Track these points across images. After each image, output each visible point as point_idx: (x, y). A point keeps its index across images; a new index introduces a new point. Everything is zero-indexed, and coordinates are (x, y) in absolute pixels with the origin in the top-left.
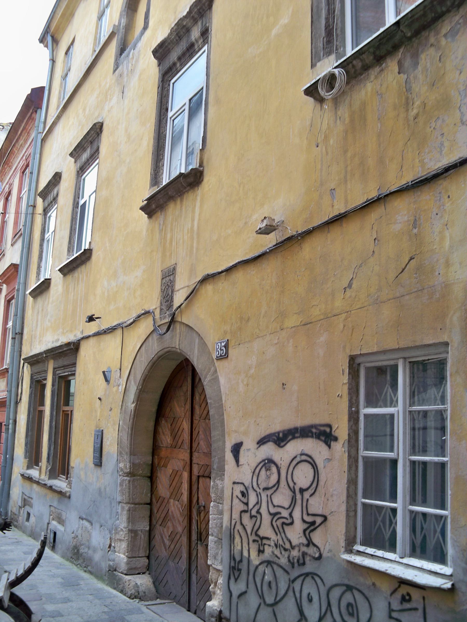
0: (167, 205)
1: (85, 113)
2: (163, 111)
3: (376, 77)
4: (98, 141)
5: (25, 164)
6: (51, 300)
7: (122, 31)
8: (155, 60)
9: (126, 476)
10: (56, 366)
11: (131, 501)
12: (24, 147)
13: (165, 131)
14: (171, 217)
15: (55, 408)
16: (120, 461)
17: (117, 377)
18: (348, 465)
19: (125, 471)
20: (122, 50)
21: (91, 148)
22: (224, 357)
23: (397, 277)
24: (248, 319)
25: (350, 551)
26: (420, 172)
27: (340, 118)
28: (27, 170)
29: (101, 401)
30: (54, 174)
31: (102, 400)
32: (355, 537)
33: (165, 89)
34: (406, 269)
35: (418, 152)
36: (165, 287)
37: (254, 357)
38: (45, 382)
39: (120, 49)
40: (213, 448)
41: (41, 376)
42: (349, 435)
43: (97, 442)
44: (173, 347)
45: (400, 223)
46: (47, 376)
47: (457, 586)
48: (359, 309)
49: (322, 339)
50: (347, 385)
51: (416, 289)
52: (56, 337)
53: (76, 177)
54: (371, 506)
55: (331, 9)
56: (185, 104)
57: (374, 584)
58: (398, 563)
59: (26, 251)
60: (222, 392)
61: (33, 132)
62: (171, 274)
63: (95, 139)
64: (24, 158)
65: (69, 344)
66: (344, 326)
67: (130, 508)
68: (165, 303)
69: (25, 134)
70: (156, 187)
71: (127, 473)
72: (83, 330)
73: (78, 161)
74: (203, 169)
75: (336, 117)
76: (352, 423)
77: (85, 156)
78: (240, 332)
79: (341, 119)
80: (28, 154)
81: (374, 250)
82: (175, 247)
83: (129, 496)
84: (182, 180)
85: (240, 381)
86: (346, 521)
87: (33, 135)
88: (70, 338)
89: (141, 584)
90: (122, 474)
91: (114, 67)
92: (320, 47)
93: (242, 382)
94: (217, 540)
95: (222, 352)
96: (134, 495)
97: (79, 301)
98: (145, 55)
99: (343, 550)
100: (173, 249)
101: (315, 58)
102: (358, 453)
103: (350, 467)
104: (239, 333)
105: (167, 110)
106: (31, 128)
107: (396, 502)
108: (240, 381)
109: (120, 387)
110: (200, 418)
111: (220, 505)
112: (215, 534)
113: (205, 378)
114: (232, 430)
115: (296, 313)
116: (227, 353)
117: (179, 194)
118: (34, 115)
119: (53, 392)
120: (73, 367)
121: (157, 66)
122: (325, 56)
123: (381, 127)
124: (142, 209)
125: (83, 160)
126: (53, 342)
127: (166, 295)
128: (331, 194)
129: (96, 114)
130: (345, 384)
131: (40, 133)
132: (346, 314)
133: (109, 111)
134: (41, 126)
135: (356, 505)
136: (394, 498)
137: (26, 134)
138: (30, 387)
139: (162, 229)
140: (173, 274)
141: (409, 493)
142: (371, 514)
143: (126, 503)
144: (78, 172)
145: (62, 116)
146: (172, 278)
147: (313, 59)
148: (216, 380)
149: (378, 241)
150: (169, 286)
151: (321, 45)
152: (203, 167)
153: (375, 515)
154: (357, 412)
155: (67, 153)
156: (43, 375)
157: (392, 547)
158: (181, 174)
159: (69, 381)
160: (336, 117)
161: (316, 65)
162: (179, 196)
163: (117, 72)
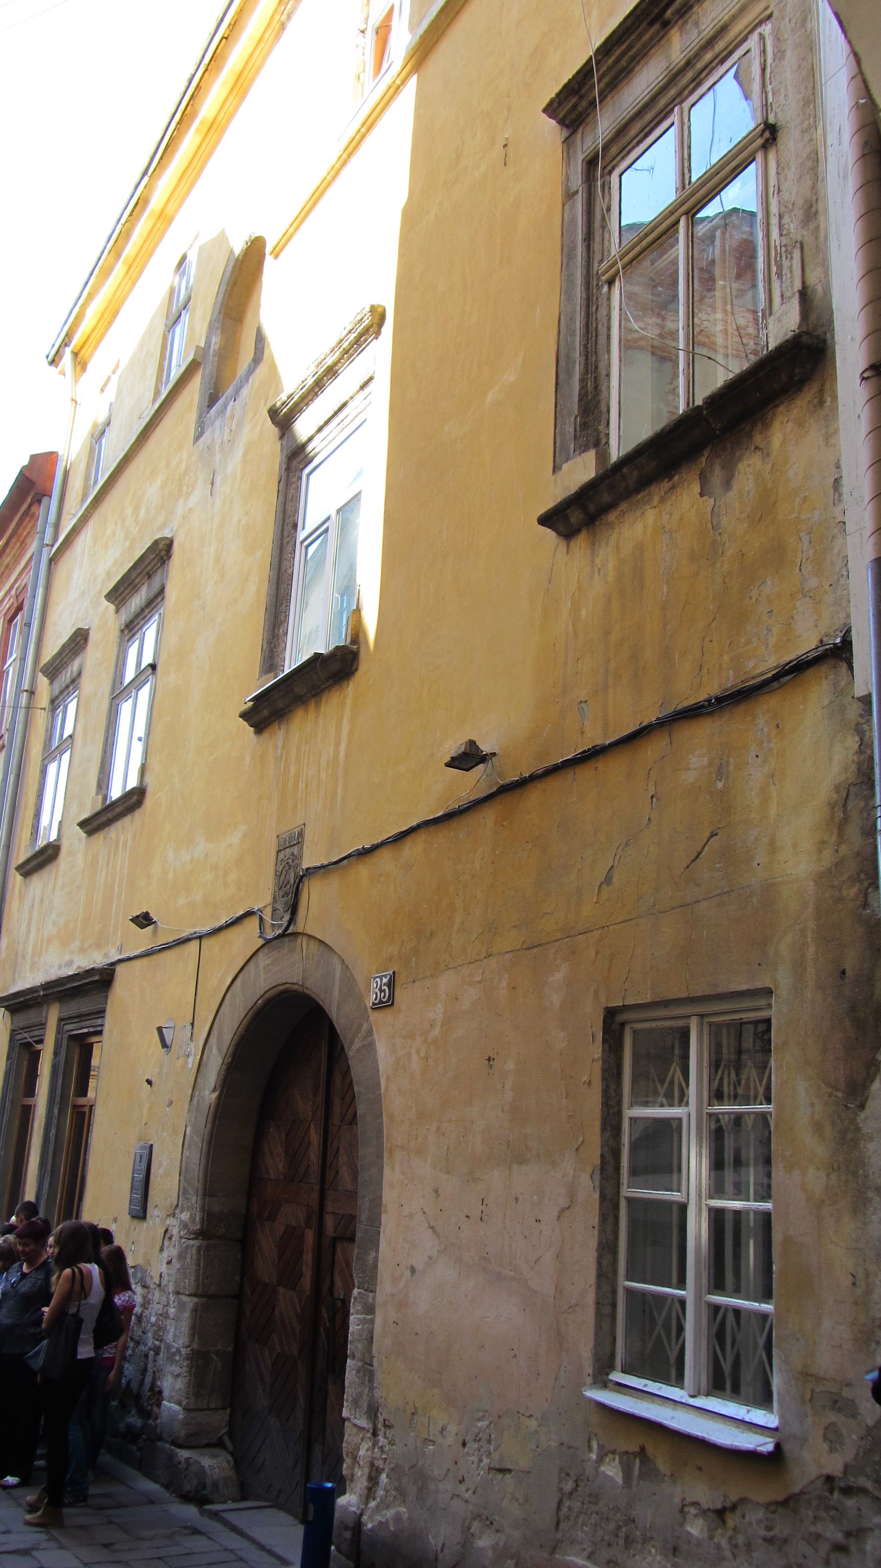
0: (290, 711)
1: (137, 516)
2: (288, 528)
3: (663, 500)
4: (162, 574)
5: (15, 605)
6: (60, 882)
7: (212, 359)
8: (273, 426)
9: (193, 1239)
10: (65, 1015)
11: (200, 1290)
12: (14, 570)
13: (290, 567)
14: (297, 734)
15: (58, 1099)
16: (182, 1207)
17: (184, 1039)
18: (599, 1214)
19: (191, 1228)
20: (212, 399)
21: (149, 586)
22: (386, 1004)
23: (688, 867)
24: (431, 934)
25: (604, 1384)
26: (731, 679)
27: (599, 570)
28: (19, 617)
29: (151, 1086)
30: (74, 630)
31: (153, 1084)
32: (613, 1355)
33: (292, 484)
34: (703, 854)
35: (728, 642)
36: (284, 868)
37: (439, 1005)
38: (39, 1047)
39: (207, 395)
40: (360, 1180)
41: (32, 1034)
42: (602, 1156)
43: (138, 1170)
44: (294, 984)
45: (695, 769)
46: (44, 1035)
47: (787, 1447)
48: (623, 922)
49: (559, 976)
50: (600, 1063)
51: (719, 891)
52: (67, 958)
53: (118, 640)
54: (644, 1294)
55: (591, 362)
56: (328, 519)
57: (643, 1449)
58: (687, 1407)
59: (14, 780)
60: (380, 1072)
61: (33, 541)
62: (295, 842)
63: (157, 570)
64: (13, 592)
65: (91, 972)
66: (597, 953)
67: (196, 1304)
68: (283, 897)
69: (15, 544)
70: (272, 674)
71: (195, 1233)
72: (122, 945)
73: (123, 610)
74: (359, 648)
75: (593, 567)
76: (608, 1134)
77: (137, 601)
78: (416, 959)
79: (602, 572)
80: (20, 585)
81: (651, 817)
82: (304, 794)
83: (197, 1280)
84: (320, 664)
85: (413, 1051)
86: (596, 1323)
87: (33, 548)
88: (97, 959)
89: (209, 1466)
90: (186, 1234)
91: (196, 430)
92: (569, 432)
93: (418, 1052)
94: (362, 1366)
95: (383, 994)
96: (207, 1278)
97: (116, 888)
98: (255, 415)
99: (589, 1380)
100: (300, 796)
101: (560, 453)
102: (618, 1192)
103: (603, 1218)
104: (414, 959)
105: (295, 526)
106: (29, 533)
107: (684, 1289)
108: (413, 1051)
109: (190, 1060)
110: (341, 1122)
111: (371, 1295)
112: (358, 1355)
113: (352, 1043)
114: (397, 1146)
115: (515, 927)
116: (392, 997)
117: (313, 693)
118: (33, 509)
119: (55, 1067)
120: (98, 1018)
121: (278, 438)
122: (577, 453)
123: (668, 592)
124: (245, 716)
125: (133, 610)
126: (60, 967)
127: (285, 883)
128: (581, 709)
129: (161, 520)
130: (597, 1060)
131: (47, 545)
132: (600, 931)
133: (184, 517)
134: (49, 532)
135: (614, 1292)
136: (682, 1283)
137: (18, 545)
138: (9, 1057)
139: (281, 757)
140: (299, 843)
141: (707, 1269)
142: (644, 1311)
143: (189, 1295)
144: (122, 631)
145: (91, 515)
146: (295, 850)
147: (557, 455)
148: (370, 1047)
149: (657, 800)
150: (290, 867)
151: (572, 430)
152: (359, 645)
153: (651, 1313)
154: (619, 1114)
155: (100, 591)
156: (36, 1033)
157: (679, 1381)
158: (317, 657)
159: (91, 1045)
160: (593, 567)
161: (560, 468)
162: (314, 696)
163: (201, 440)
